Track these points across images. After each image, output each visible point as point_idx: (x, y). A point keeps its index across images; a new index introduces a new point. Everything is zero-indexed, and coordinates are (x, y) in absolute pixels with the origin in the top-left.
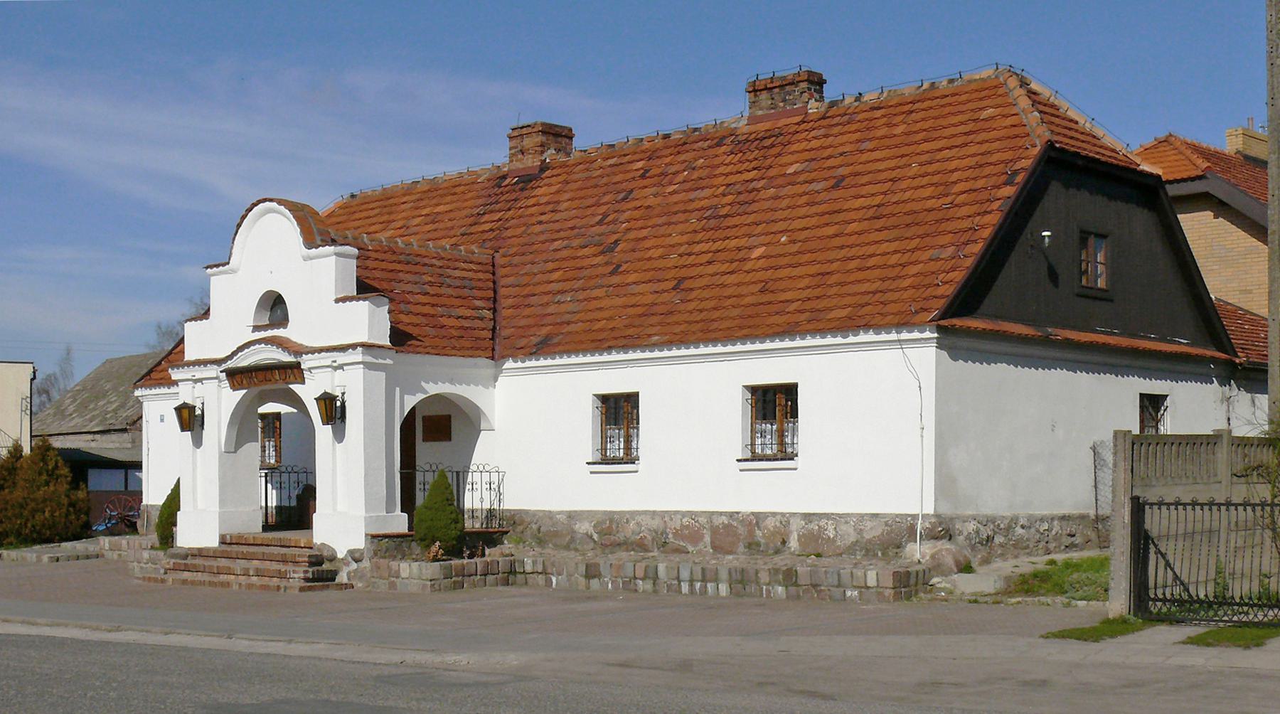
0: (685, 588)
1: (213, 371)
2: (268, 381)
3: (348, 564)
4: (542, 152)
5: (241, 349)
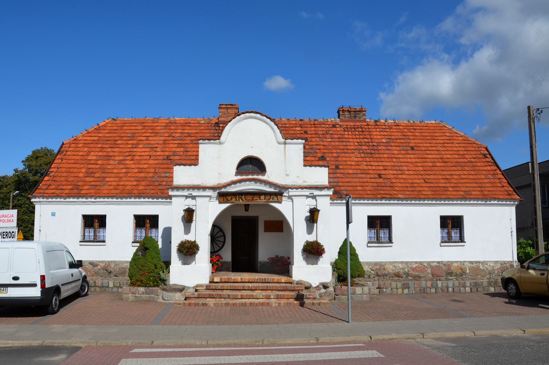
0: (450, 289)
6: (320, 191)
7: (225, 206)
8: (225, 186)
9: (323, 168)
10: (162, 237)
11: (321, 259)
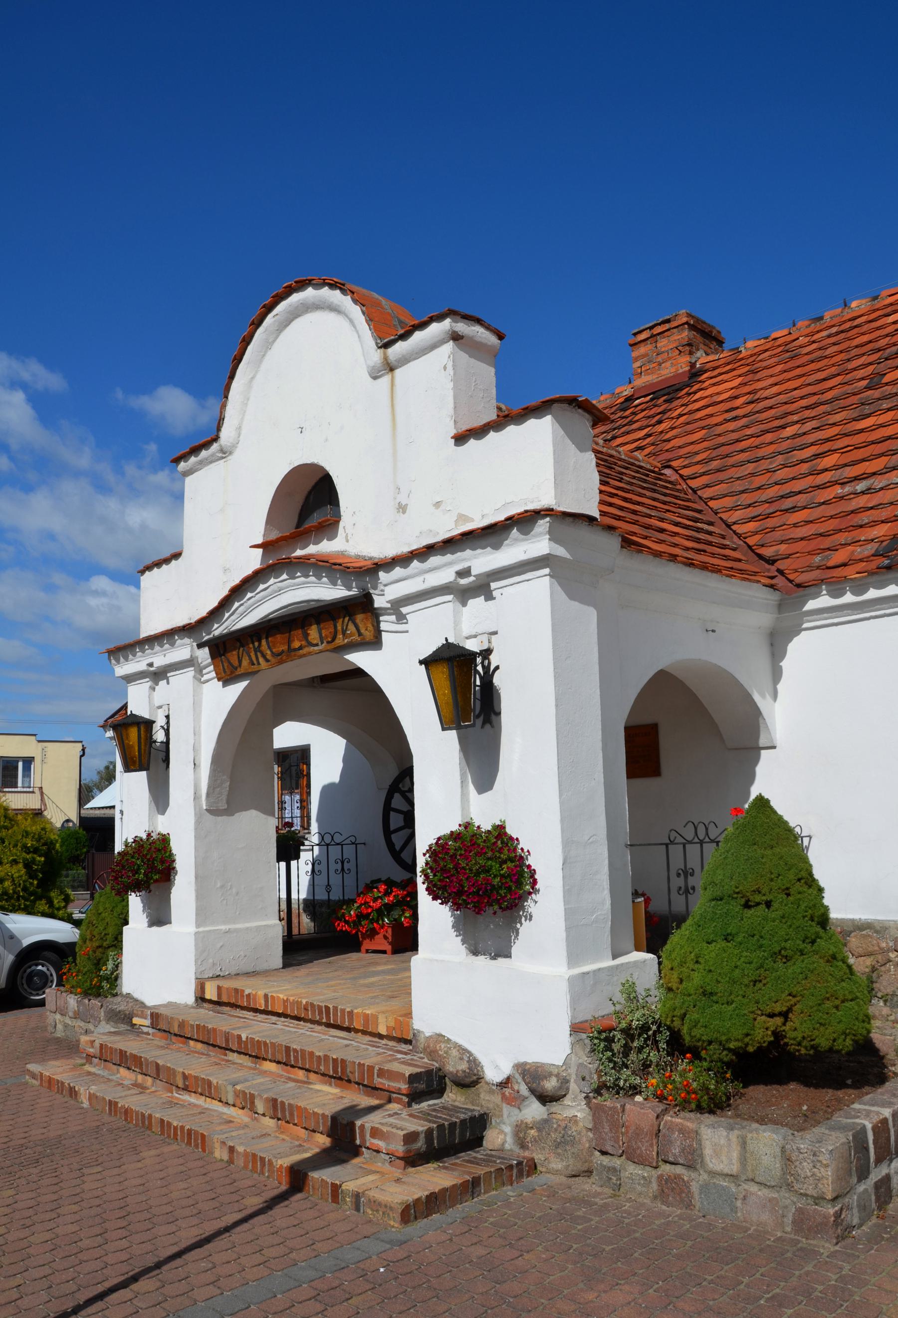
1: (183, 650)
2: (290, 654)
3: (516, 1101)
4: (691, 353)
5: (237, 592)
6: (497, 547)
7: (239, 687)
8: (216, 613)
9: (532, 423)
10: (318, 820)
11: (525, 928)
